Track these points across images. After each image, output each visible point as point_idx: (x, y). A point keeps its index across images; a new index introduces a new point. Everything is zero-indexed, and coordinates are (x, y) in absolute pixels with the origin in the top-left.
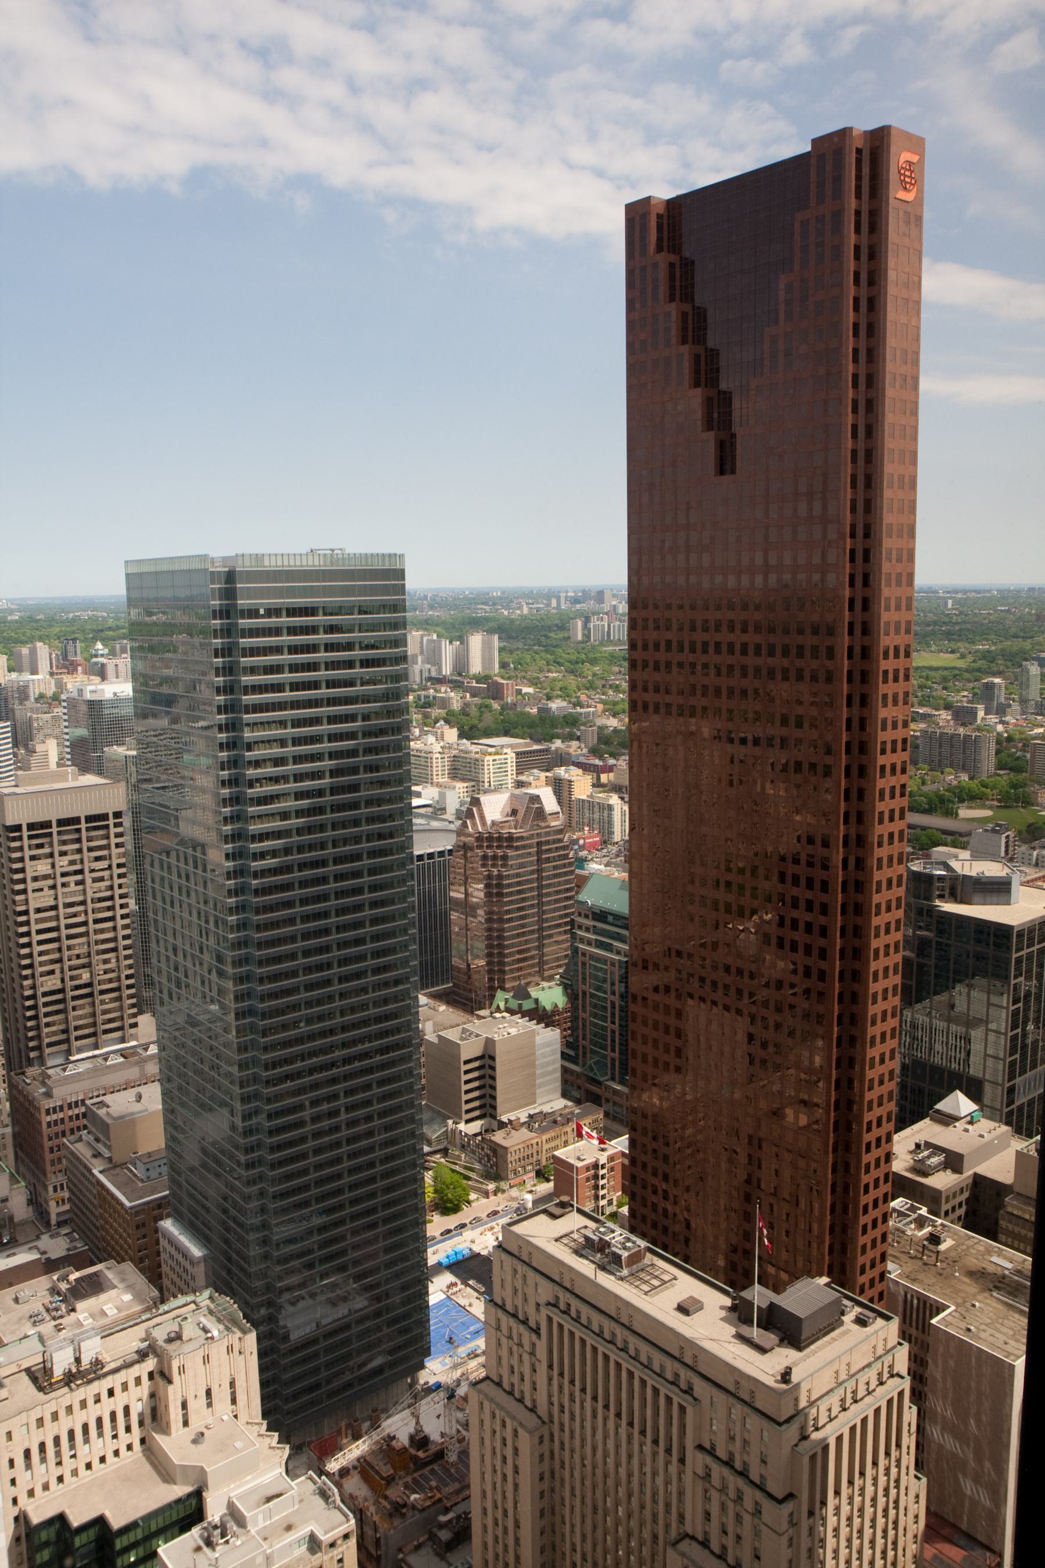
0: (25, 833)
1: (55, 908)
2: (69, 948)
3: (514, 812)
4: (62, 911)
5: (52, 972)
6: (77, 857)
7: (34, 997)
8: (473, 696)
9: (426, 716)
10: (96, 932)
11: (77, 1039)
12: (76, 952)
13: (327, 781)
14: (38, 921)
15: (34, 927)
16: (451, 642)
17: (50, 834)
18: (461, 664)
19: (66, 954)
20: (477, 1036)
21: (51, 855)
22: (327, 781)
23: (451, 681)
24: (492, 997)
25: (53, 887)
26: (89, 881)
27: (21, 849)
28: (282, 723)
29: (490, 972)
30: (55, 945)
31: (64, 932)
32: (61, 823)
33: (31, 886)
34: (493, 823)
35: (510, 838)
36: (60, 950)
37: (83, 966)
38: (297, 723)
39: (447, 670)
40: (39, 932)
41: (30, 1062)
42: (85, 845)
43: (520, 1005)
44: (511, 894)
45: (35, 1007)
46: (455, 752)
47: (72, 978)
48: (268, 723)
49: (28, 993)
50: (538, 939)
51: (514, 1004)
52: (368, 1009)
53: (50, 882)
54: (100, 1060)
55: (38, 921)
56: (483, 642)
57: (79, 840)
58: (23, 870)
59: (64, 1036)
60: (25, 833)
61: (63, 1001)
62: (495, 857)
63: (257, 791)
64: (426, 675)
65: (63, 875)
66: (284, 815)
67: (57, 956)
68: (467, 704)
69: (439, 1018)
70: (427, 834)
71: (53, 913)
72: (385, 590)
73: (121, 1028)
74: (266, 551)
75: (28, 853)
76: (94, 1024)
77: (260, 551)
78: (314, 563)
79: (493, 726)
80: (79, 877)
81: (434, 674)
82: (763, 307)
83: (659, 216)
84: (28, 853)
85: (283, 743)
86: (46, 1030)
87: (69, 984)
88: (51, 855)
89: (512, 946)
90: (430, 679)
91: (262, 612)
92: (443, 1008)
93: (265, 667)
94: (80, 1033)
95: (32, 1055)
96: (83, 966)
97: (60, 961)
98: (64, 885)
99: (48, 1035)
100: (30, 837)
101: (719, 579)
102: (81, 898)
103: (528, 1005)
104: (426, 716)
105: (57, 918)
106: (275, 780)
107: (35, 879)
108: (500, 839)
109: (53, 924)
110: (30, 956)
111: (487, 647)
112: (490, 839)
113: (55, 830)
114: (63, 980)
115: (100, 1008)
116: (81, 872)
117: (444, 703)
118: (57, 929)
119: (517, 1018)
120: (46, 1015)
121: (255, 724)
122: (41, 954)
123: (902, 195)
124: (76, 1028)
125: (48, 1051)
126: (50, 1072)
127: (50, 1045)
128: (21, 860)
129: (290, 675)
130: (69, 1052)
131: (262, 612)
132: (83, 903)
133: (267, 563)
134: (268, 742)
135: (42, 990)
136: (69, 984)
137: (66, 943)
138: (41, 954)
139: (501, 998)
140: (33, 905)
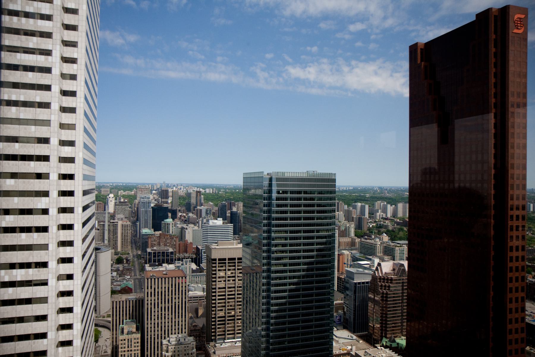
0: (217, 262)
1: (225, 288)
2: (228, 302)
3: (394, 270)
4: (227, 289)
5: (222, 310)
6: (234, 271)
7: (215, 318)
8: (397, 225)
9: (379, 231)
10: (237, 298)
11: (228, 334)
12: (230, 304)
13: (315, 253)
14: (219, 292)
15: (218, 294)
16: (391, 205)
17: (225, 263)
18: (395, 214)
19: (227, 304)
20: (370, 355)
21: (225, 270)
22: (315, 253)
23: (390, 219)
24: (381, 340)
25: (225, 281)
26: (237, 280)
27: (216, 267)
28: (286, 232)
29: (382, 330)
30: (224, 301)
31: (227, 297)
32: (229, 259)
33: (218, 280)
34: (386, 273)
35: (392, 279)
36: (225, 303)
37: (232, 309)
38: (291, 232)
39: (389, 215)
40: (219, 296)
41: (212, 341)
42: (237, 267)
43: (391, 345)
44: (391, 301)
45: (215, 321)
46: (385, 245)
47: (228, 313)
48: (281, 231)
49: (213, 316)
50: (401, 319)
51: (388, 344)
52: (299, 342)
53: (224, 279)
54: (234, 343)
55: (219, 292)
56: (403, 206)
57: (235, 266)
58: (215, 274)
59: (224, 333)
60: (217, 262)
61: (224, 320)
62: (385, 286)
63: (275, 255)
64: (381, 216)
65: (229, 277)
66: (285, 265)
67: (224, 305)
68: (395, 228)
69: (359, 345)
70: (362, 275)
71: (224, 290)
72: (328, 186)
73: (234, 334)
74: (286, 171)
75: (218, 268)
76: (234, 330)
77: (284, 171)
78: (305, 176)
79: (403, 236)
80: (234, 278)
81: (384, 216)
82: (454, 79)
83: (421, 49)
84: (218, 268)
85: (286, 239)
86: (218, 330)
87: (227, 315)
88: (225, 270)
89: (390, 321)
90: (382, 218)
91: (281, 192)
92: (361, 341)
93: (281, 211)
94: (229, 332)
95: (213, 338)
96: (232, 309)
97: (225, 306)
98: (228, 281)
99: (218, 332)
100: (219, 263)
101: (442, 185)
102: (234, 286)
103: (394, 345)
104: (379, 231)
105: (225, 292)
106: (282, 252)
107: (219, 277)
108: (388, 279)
109: (224, 293)
110: (215, 303)
111: (404, 208)
112: (384, 279)
113: (227, 261)
114: (225, 313)
115: (237, 325)
116: (234, 277)
117: (386, 227)
118: (225, 295)
119: (387, 350)
120: (219, 325)
121: (276, 231)
122: (219, 303)
123: (516, 31)
124: (228, 331)
125: (218, 337)
126: (217, 345)
127: (219, 335)
128: (215, 270)
129: (292, 214)
130: (224, 339)
131: (281, 192)
132: (234, 287)
133: (286, 175)
134: (281, 238)
135: (218, 316)
136: (227, 315)
137: (227, 300)
138: (219, 303)
139: (385, 341)
140: (218, 286)
